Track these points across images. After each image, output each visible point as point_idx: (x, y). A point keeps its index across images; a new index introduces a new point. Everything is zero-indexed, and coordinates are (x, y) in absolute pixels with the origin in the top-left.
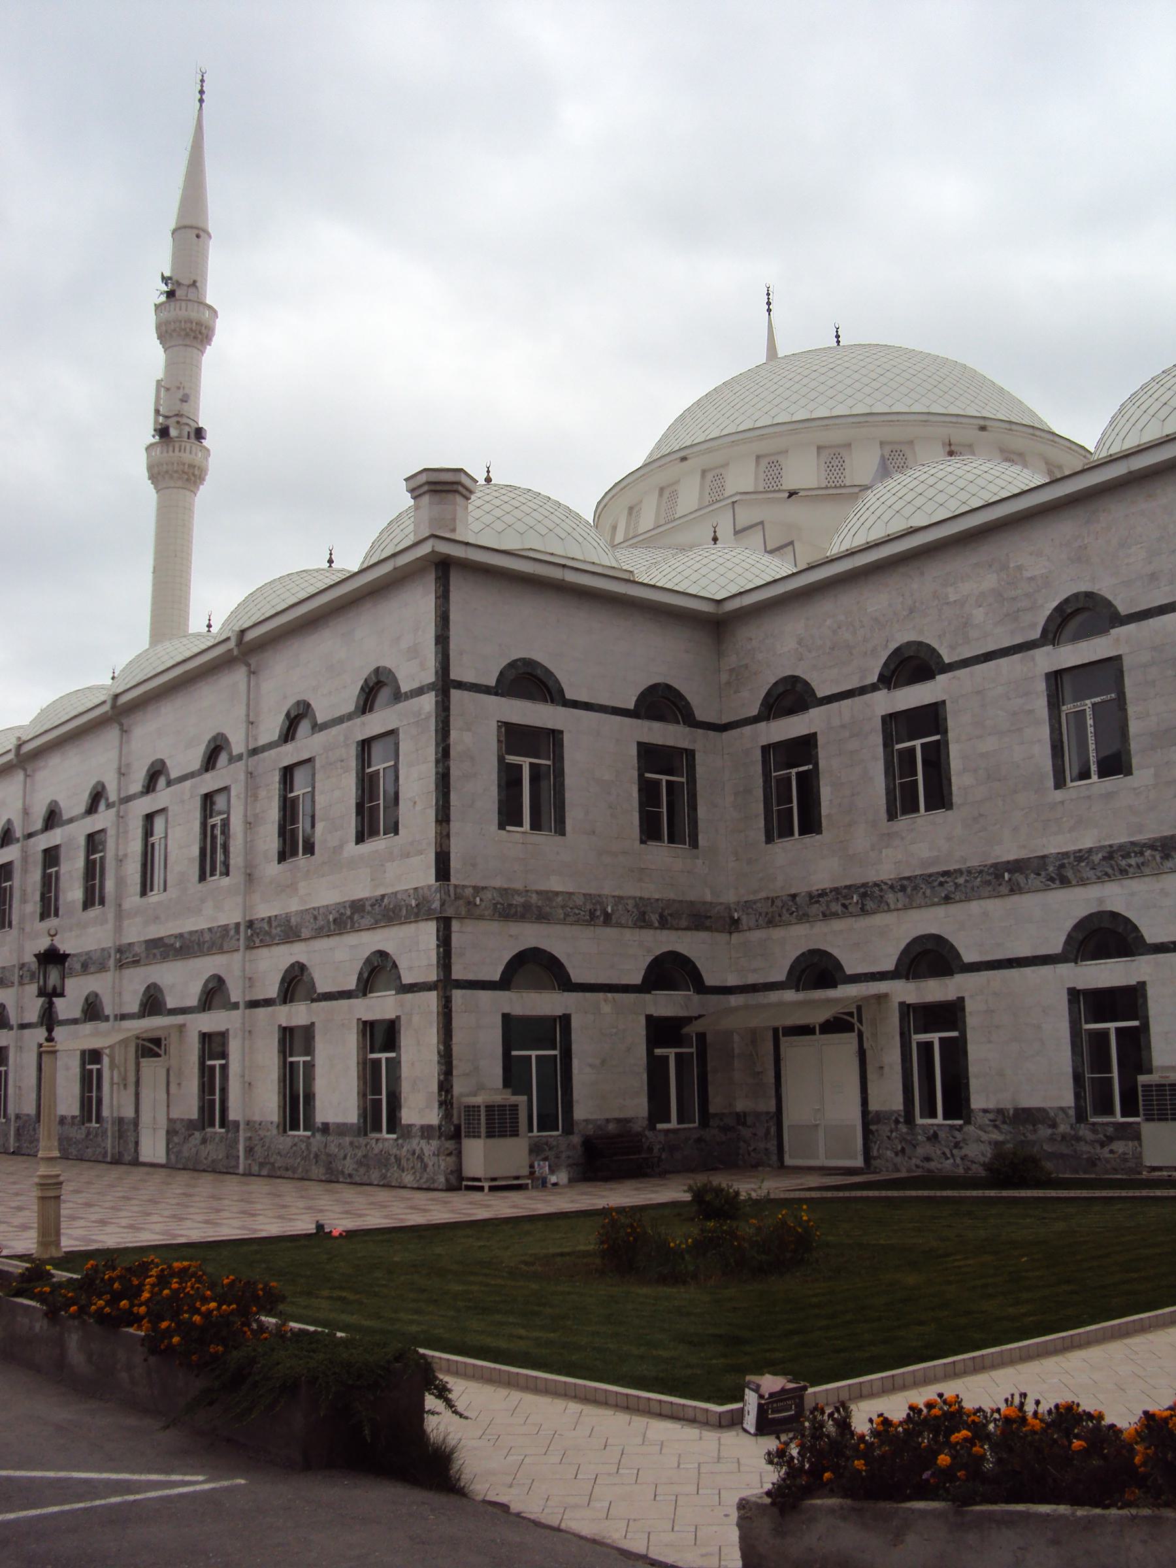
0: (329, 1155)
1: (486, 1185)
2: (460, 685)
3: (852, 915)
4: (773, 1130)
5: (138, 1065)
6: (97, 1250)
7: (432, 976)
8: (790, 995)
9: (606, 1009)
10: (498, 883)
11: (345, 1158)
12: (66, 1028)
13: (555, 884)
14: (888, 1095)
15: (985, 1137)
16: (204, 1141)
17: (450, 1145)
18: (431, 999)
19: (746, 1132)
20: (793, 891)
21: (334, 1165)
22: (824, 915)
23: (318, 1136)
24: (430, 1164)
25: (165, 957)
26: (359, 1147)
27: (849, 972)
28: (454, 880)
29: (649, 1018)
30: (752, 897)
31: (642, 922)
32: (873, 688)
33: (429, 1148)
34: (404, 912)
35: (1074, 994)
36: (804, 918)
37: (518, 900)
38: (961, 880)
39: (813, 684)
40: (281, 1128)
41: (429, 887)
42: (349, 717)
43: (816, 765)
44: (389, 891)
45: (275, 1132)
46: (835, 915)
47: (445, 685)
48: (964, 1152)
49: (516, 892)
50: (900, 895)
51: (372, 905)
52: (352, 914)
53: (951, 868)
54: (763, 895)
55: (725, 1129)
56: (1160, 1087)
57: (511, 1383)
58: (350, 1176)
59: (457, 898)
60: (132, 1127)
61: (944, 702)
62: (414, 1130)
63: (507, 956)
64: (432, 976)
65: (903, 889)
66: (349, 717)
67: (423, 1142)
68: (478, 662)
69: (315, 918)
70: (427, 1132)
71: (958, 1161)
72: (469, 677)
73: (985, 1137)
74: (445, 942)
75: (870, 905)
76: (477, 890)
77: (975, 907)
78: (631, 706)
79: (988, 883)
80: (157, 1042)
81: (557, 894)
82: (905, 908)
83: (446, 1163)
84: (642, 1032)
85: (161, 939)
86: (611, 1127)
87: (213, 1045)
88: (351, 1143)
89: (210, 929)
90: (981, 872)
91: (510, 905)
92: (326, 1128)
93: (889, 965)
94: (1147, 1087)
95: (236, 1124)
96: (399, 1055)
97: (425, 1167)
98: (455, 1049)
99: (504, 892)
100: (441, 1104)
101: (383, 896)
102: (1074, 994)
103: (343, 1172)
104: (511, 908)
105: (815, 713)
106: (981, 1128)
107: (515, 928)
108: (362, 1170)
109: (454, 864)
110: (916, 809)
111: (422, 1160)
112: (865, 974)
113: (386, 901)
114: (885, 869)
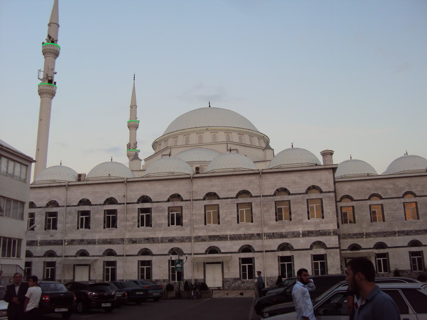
36: (352, 238)
46: (360, 238)
65: (375, 234)
66: (303, 194)
77: (390, 238)
101: (320, 231)
114: (371, 230)
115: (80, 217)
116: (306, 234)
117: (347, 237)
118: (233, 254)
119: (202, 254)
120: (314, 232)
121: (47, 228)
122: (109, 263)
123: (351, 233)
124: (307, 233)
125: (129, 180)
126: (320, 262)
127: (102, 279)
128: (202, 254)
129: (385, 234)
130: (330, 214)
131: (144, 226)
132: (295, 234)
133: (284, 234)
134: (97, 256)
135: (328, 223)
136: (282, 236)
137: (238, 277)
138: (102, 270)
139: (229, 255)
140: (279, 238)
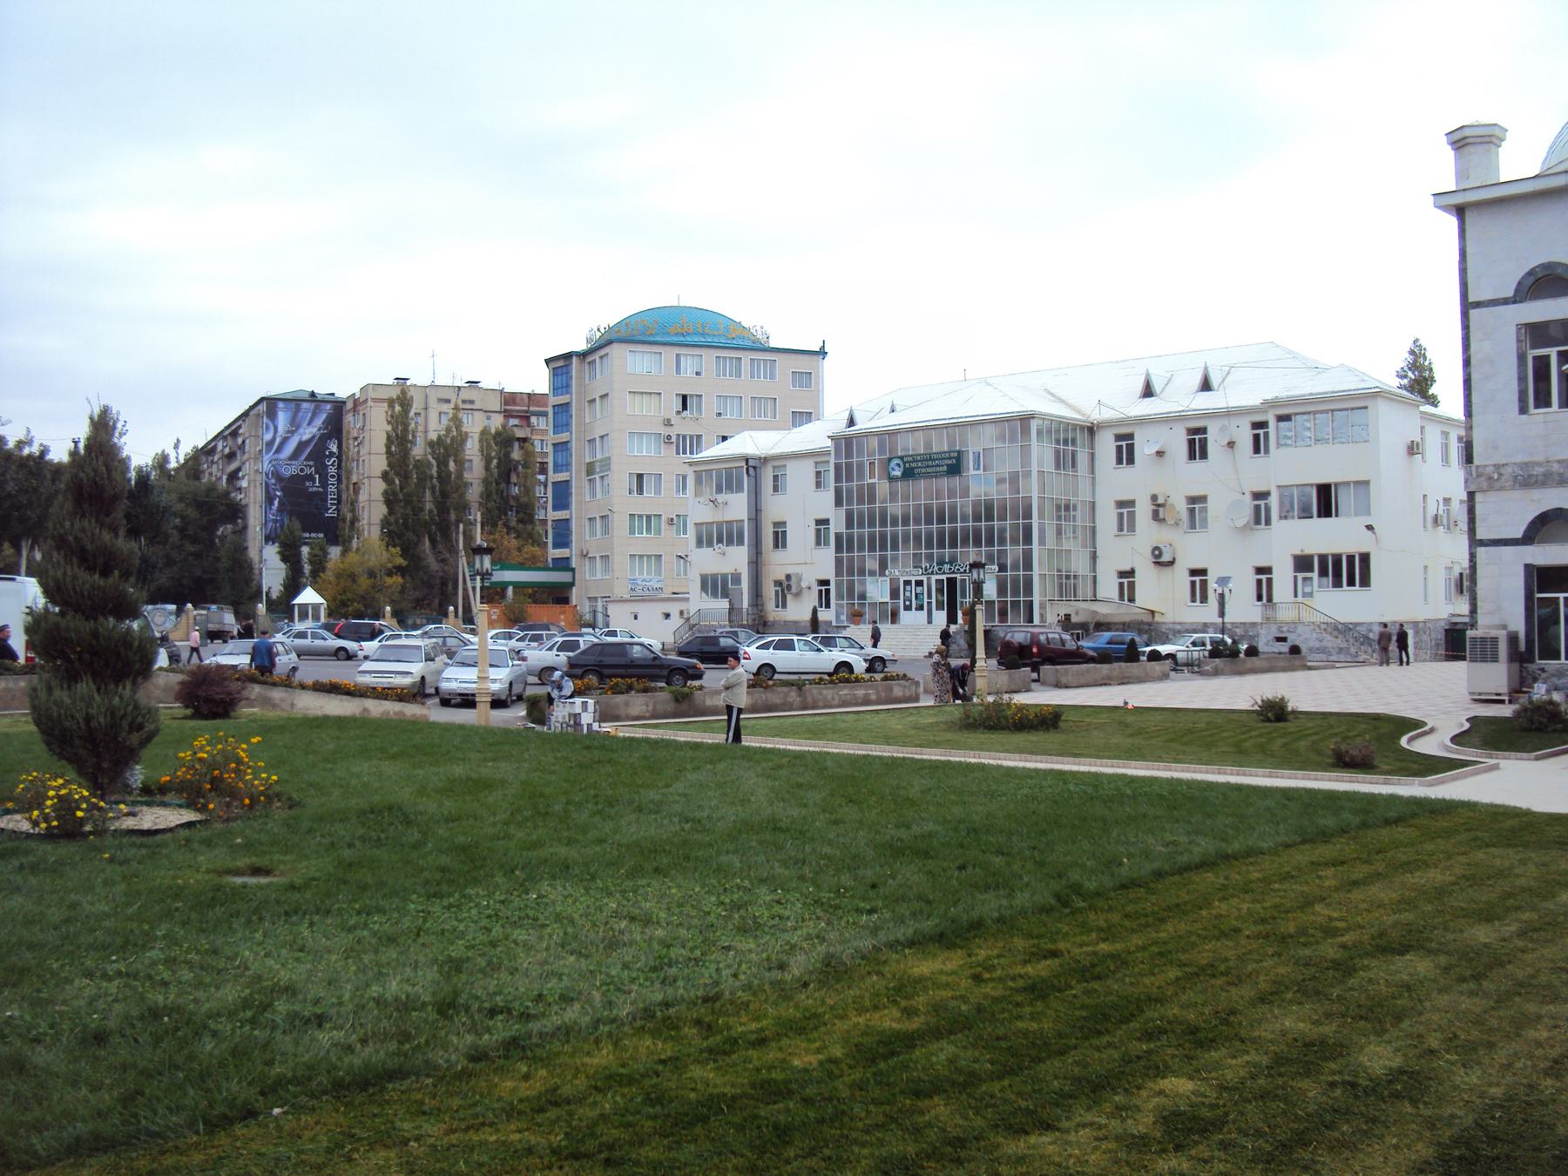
10: (1519, 459)
12: (1466, 556)
28: (1476, 462)
29: (1528, 567)
35: (1529, 568)
37: (1539, 470)
42: (1505, 301)
49: (1539, 464)
56: (1483, 639)
57: (1454, 779)
63: (1530, 517)
66: (1505, 301)
76: (1497, 467)
91: (1530, 476)
94: (1473, 639)
99: (1525, 465)
102: (1529, 568)
104: (1528, 479)
107: (1536, 494)
110: (1548, 404)
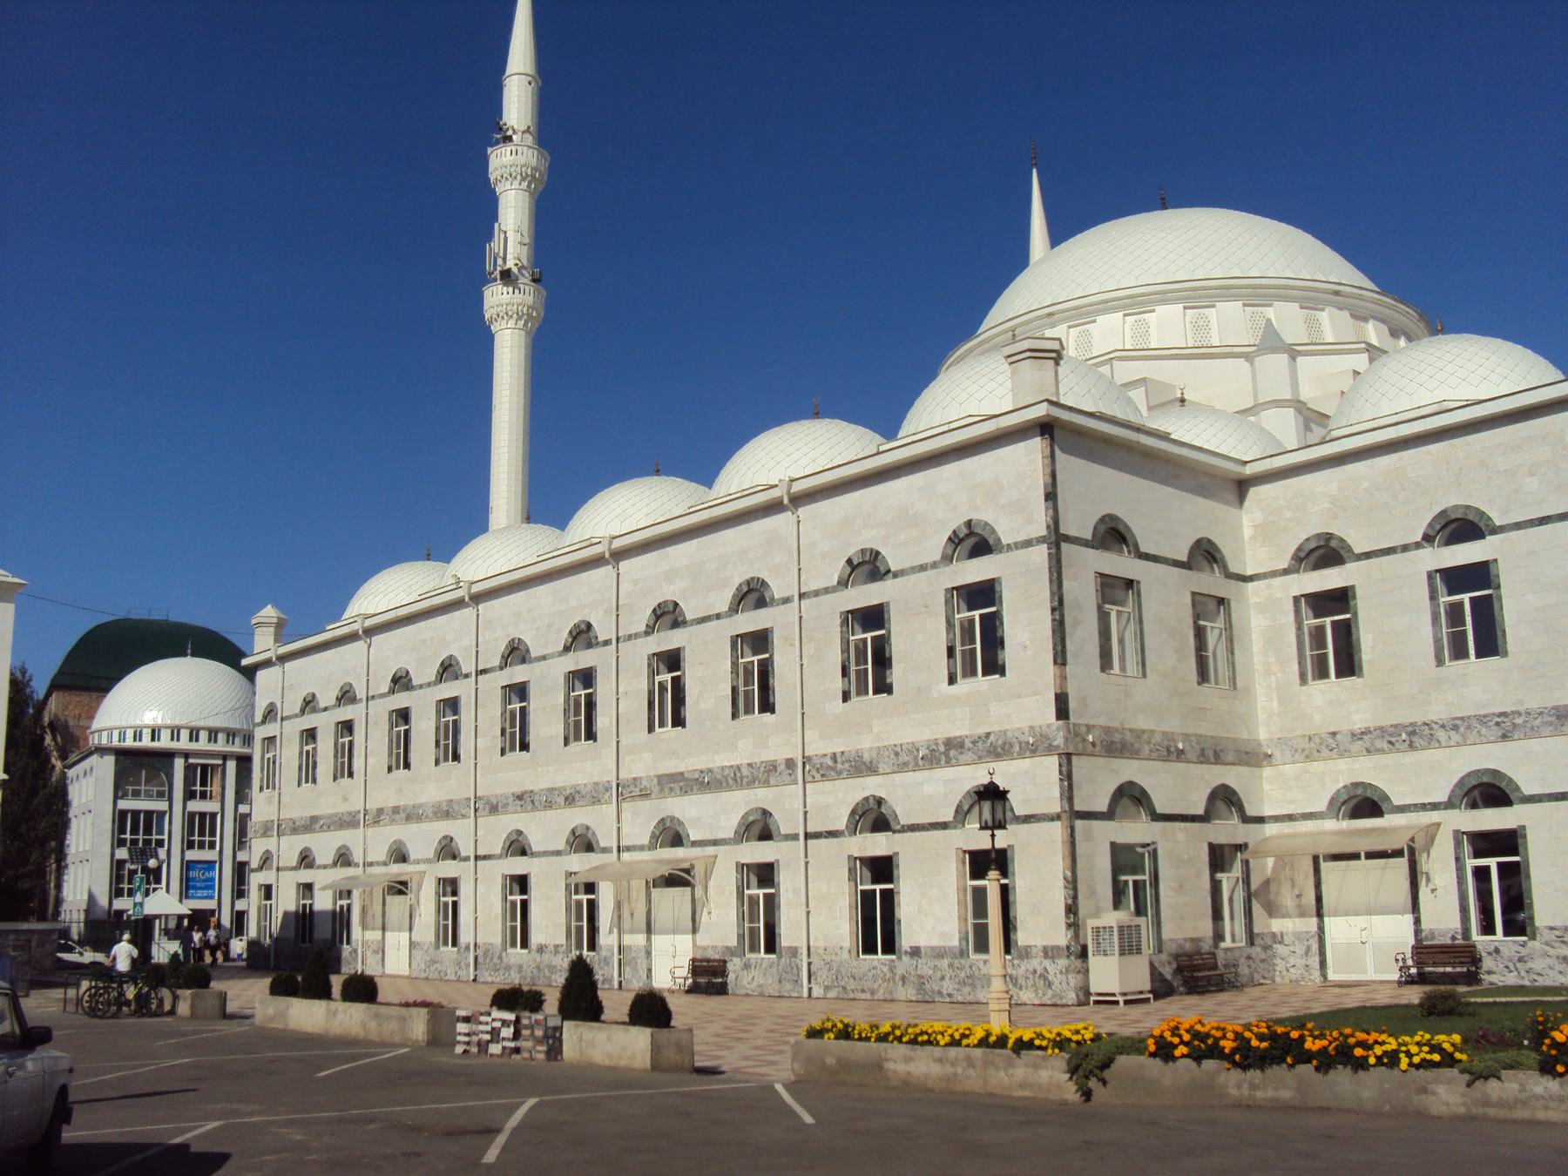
0: (920, 977)
1: (1121, 999)
2: (1068, 539)
3: (1399, 751)
4: (1315, 947)
5: (649, 895)
6: (1362, 1009)
7: (1055, 807)
8: (1330, 825)
9: (1181, 836)
11: (943, 978)
13: (1142, 723)
14: (1444, 912)
15: (1551, 951)
16: (747, 966)
17: (1078, 963)
18: (1057, 830)
19: (1279, 948)
20: (1332, 729)
21: (927, 986)
22: (1368, 751)
23: (905, 959)
24: (1056, 982)
25: (685, 791)
26: (961, 968)
27: (1396, 803)
30: (1286, 735)
31: (1203, 758)
32: (1417, 545)
33: (1055, 968)
34: (1017, 748)
36: (1344, 753)
38: (1519, 721)
39: (1350, 541)
40: (854, 952)
41: (1049, 726)
43: (1355, 614)
44: (995, 728)
45: (845, 955)
46: (1381, 751)
47: (1057, 539)
48: (1529, 965)
49: (1116, 730)
50: (1452, 733)
51: (974, 743)
52: (948, 750)
53: (1508, 710)
54: (1299, 732)
55: (1266, 948)
58: (950, 995)
59: (1076, 735)
60: (643, 954)
61: (1496, 561)
62: (1034, 950)
64: (1055, 807)
65: (1455, 728)
66: (935, 565)
67: (1047, 963)
68: (1079, 523)
69: (897, 754)
70: (1049, 952)
71: (1523, 973)
72: (1072, 532)
73: (1551, 951)
74: (1067, 776)
75: (1417, 741)
77: (1534, 744)
78: (1184, 558)
79: (1551, 724)
80: (404, 883)
81: (1143, 731)
82: (1458, 745)
83: (1074, 980)
84: (1206, 858)
85: (682, 774)
86: (1188, 946)
87: (450, 886)
88: (951, 965)
89: (750, 765)
90: (1540, 714)
92: (915, 952)
93: (1442, 797)
95: (794, 952)
96: (778, 891)
97: (1050, 985)
98: (1079, 874)
100: (1069, 926)
101: (988, 734)
103: (940, 993)
105: (1351, 567)
106: (1547, 944)
108: (967, 989)
109: (1072, 704)
110: (1465, 655)
111: (1045, 979)
112: (1415, 805)
113: (992, 738)
114: (1437, 710)
115: (1445, 599)
116: (947, 752)
117: (1325, 753)
118: (721, 849)
119: (642, 848)
120: (968, 744)
121: (738, 706)
122: (1486, 843)
123: (1343, 727)
124: (942, 749)
125: (797, 487)
126: (1499, 864)
127: (1455, 923)
128: (642, 848)
129: (1506, 726)
130: (1029, 653)
131: (1465, 655)
132: (904, 758)
133: (866, 757)
134: (1424, 807)
135: (1019, 696)
136: (862, 767)
137: (733, 942)
138: (432, 908)
139: (711, 850)
140: (851, 776)
